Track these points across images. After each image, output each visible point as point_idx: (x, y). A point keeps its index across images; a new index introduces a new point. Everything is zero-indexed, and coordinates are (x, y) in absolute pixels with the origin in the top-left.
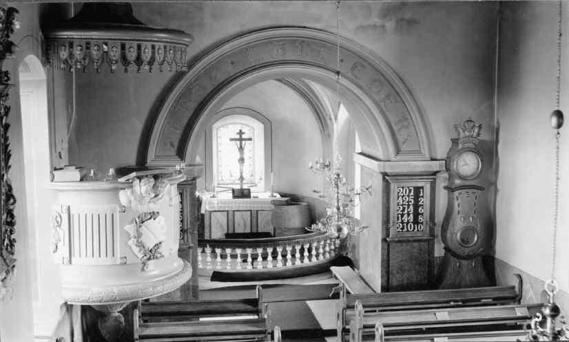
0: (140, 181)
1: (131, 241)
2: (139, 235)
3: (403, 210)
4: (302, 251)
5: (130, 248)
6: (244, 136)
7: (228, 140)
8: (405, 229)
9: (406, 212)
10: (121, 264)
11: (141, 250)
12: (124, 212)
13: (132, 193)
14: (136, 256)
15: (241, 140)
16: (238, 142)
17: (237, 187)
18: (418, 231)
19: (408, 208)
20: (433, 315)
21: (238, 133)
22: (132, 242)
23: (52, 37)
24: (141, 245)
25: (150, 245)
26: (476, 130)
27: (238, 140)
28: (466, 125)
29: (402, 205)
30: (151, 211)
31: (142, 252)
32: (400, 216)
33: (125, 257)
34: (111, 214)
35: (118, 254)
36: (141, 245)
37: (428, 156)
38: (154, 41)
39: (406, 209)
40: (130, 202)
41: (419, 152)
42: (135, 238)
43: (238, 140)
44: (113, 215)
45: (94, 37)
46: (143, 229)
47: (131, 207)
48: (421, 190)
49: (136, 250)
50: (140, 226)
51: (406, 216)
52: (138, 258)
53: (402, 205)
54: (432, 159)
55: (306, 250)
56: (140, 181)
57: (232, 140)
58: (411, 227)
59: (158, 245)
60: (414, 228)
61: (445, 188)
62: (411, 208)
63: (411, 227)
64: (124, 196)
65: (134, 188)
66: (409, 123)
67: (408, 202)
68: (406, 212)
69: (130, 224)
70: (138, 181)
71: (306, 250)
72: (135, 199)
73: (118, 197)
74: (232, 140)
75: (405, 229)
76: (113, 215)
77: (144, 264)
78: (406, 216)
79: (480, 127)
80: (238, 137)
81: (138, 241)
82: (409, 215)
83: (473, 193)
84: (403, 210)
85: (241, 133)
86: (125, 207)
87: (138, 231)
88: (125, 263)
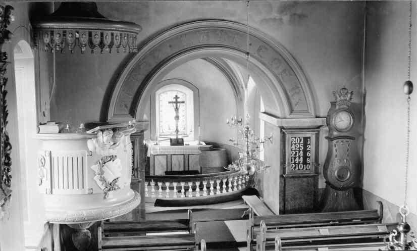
0: (103, 133)
2: (102, 173)
3: (296, 154)
4: (221, 184)
5: (96, 182)
6: (179, 100)
8: (297, 168)
9: (297, 155)
10: (89, 194)
11: (103, 183)
12: (91, 155)
13: (97, 141)
14: (100, 188)
15: (177, 102)
16: (175, 105)
17: (174, 137)
18: (306, 169)
20: (317, 231)
21: (174, 98)
22: (97, 178)
23: (38, 27)
24: (103, 180)
25: (110, 180)
26: (349, 95)
27: (175, 102)
28: (342, 92)
29: (295, 151)
30: (111, 155)
31: (104, 185)
32: (293, 158)
34: (81, 157)
35: (87, 187)
36: (103, 180)
37: (314, 115)
38: (113, 30)
39: (298, 154)
40: (95, 148)
41: (307, 112)
42: (99, 174)
43: (175, 102)
44: (83, 158)
45: (69, 27)
46: (105, 168)
47: (96, 152)
48: (309, 140)
49: (100, 183)
50: (103, 166)
52: (101, 189)
53: (295, 151)
54: (317, 117)
55: (224, 183)
56: (103, 133)
57: (170, 102)
58: (301, 166)
59: (115, 180)
60: (304, 168)
61: (326, 138)
62: (302, 152)
63: (301, 166)
64: (91, 144)
65: (98, 138)
66: (300, 91)
67: (299, 148)
68: (297, 155)
69: (95, 164)
70: (101, 133)
71: (224, 183)
72: (99, 146)
73: (87, 145)
74: (170, 102)
75: (297, 168)
76: (83, 158)
77: (106, 194)
78: (297, 158)
79: (352, 93)
80: (174, 100)
81: (101, 177)
82: (299, 157)
83: (347, 142)
84: (296, 154)
85: (176, 97)
87: (101, 169)
88: (92, 193)
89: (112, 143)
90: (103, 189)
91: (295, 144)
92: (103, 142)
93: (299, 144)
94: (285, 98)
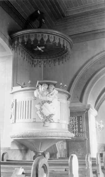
0: (41, 86)
1: (38, 112)
2: (41, 109)
3: (73, 126)
7: (16, 98)
8: (80, 135)
9: (74, 127)
10: (33, 122)
11: (42, 116)
12: (36, 99)
14: (40, 119)
18: (81, 136)
19: (75, 126)
22: (38, 113)
23: (13, 37)
24: (42, 114)
29: (73, 124)
30: (48, 100)
31: (43, 117)
32: (72, 129)
33: (35, 119)
34: (30, 101)
35: (32, 117)
36: (42, 114)
38: (43, 33)
39: (75, 126)
40: (38, 95)
42: (39, 110)
44: (31, 101)
45: (25, 33)
46: (43, 107)
47: (38, 98)
48: (81, 118)
49: (40, 116)
51: (75, 129)
52: (41, 120)
53: (73, 124)
56: (41, 86)
58: (77, 133)
59: (51, 116)
60: (79, 134)
62: (77, 126)
63: (77, 133)
64: (36, 93)
65: (39, 89)
67: (75, 123)
68: (74, 127)
69: (37, 105)
70: (40, 86)
72: (40, 93)
73: (34, 94)
75: (80, 135)
76: (31, 101)
77: (44, 122)
78: (75, 129)
81: (40, 112)
82: (76, 129)
84: (73, 126)
86: (36, 97)
88: (35, 121)
89: (48, 93)
90: (42, 119)
91: (73, 120)
92: (42, 91)
93: (75, 120)
94: (71, 89)
